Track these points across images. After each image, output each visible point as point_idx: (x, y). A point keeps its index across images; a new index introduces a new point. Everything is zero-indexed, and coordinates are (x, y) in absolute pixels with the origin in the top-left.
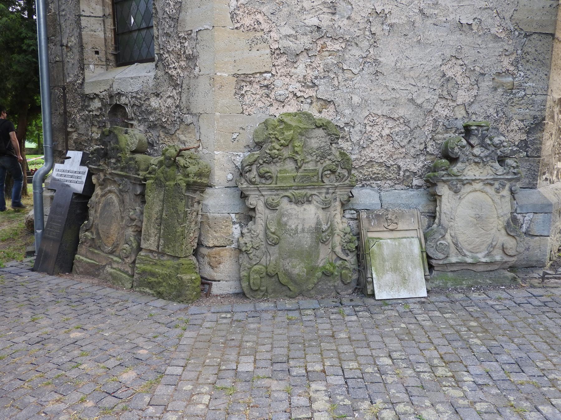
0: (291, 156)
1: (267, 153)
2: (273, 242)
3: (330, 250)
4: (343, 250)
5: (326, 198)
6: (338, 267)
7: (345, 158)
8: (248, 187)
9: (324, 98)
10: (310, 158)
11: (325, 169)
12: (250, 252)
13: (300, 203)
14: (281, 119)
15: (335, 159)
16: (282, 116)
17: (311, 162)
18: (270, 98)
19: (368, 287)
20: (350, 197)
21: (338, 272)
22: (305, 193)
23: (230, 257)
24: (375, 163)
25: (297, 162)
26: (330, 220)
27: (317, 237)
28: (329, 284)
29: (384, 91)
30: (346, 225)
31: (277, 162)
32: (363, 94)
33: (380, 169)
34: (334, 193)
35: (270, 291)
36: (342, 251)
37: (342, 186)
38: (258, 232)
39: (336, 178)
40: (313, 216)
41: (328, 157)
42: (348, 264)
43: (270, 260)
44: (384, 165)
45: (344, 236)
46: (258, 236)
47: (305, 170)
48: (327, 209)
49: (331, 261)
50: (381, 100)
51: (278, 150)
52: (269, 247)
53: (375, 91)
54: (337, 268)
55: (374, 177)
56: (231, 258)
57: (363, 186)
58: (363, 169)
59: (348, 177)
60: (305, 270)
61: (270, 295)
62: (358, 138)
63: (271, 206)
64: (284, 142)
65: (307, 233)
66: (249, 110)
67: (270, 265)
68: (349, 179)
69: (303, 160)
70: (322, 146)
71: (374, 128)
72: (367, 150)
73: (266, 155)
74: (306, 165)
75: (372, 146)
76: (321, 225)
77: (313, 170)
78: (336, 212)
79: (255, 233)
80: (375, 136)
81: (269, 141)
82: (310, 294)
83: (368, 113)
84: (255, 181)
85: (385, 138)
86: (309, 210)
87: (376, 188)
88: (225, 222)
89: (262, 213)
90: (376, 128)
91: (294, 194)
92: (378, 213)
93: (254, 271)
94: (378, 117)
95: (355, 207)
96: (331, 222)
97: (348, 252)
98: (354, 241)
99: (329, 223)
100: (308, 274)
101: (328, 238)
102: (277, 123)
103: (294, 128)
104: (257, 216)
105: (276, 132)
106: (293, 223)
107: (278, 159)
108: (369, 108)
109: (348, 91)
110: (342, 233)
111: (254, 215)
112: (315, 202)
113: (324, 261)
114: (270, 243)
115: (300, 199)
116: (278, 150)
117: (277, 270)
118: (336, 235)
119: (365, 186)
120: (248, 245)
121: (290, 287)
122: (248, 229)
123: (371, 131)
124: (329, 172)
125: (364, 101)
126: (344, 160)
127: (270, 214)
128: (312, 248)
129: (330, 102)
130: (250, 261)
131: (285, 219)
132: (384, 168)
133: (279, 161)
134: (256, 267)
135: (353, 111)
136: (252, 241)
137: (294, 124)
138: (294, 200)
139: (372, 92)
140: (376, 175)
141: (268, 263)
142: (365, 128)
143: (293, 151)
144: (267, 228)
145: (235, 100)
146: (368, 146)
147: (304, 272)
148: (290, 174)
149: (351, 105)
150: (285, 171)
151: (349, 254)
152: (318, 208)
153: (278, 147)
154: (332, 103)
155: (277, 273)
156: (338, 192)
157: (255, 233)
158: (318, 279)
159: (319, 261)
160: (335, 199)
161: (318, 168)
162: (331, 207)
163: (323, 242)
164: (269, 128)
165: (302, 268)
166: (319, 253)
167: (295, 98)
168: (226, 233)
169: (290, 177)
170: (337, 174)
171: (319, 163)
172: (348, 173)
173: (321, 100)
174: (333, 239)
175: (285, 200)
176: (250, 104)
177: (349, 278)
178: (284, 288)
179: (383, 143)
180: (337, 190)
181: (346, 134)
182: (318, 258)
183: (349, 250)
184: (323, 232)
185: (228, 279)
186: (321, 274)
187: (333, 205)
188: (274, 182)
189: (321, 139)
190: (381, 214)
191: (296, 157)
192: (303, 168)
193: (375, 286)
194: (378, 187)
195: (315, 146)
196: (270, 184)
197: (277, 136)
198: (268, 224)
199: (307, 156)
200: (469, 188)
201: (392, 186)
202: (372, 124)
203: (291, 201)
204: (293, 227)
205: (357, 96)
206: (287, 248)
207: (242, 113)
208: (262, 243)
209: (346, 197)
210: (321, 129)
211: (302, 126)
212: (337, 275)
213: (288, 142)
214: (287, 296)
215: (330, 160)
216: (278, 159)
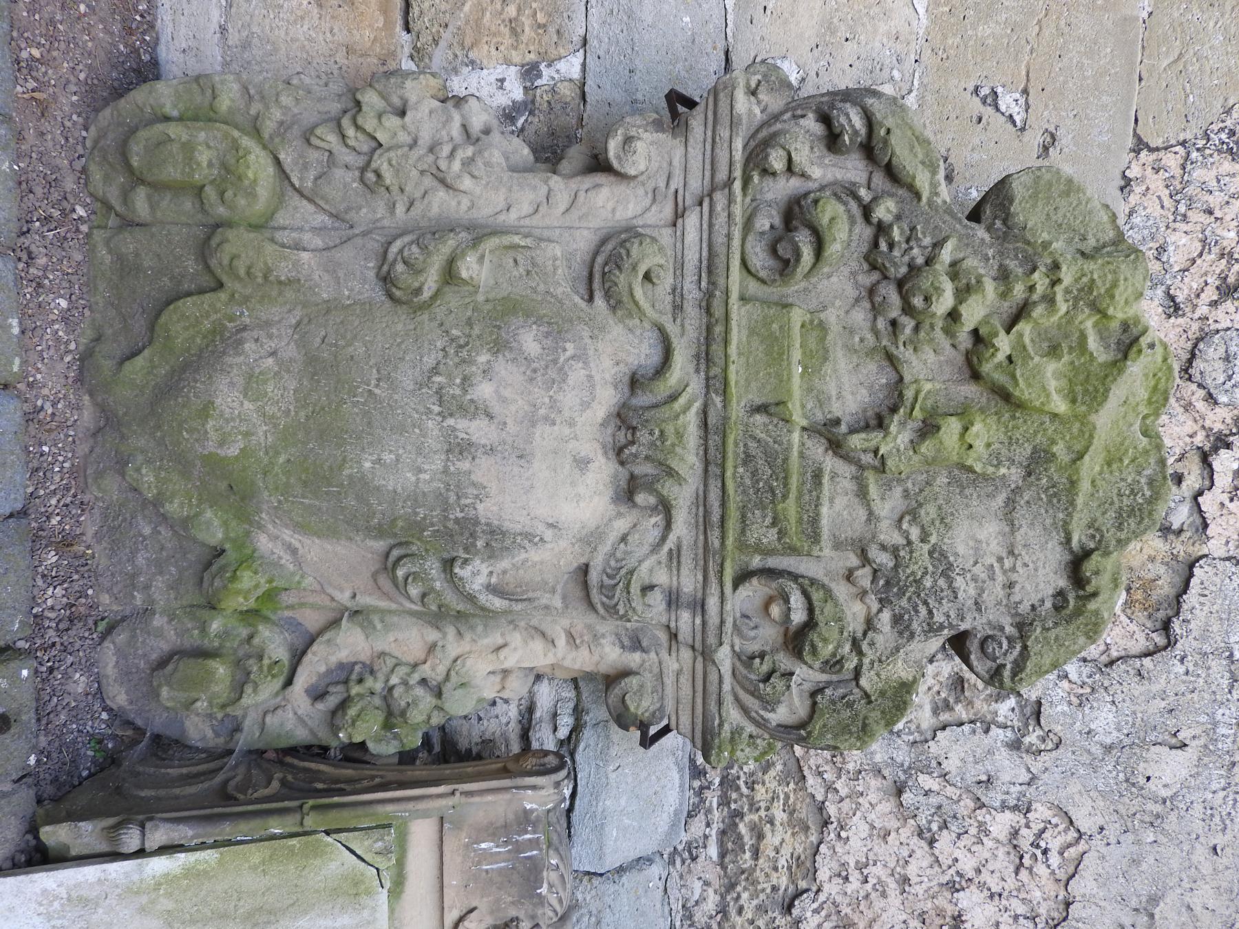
0: (909, 394)
1: (938, 245)
2: (400, 267)
3: (344, 597)
4: (345, 674)
5: (647, 589)
6: (251, 637)
7: (876, 715)
8: (734, 123)
9: (1191, 598)
10: (887, 506)
11: (817, 596)
12: (350, 132)
13: (622, 437)
14: (1144, 341)
15: (870, 655)
16: (1159, 350)
17: (862, 514)
18: (1214, 304)
19: (86, 826)
20: (643, 726)
21: (225, 634)
22: (682, 469)
23: (349, 50)
24: (814, 838)
25: (867, 427)
26: (518, 607)
27: (417, 527)
28: (159, 583)
29: (1206, 917)
30: (489, 694)
31: (876, 310)
32: (1198, 807)
33: (782, 862)
34: (673, 636)
35: (129, 243)
36: (341, 666)
37: (713, 688)
38: (467, 183)
39: (762, 656)
40: (543, 511)
41: (886, 616)
42: (268, 690)
43: (298, 247)
44: (803, 884)
45: (423, 682)
46: (443, 182)
47: (817, 476)
48: (578, 593)
49: (288, 599)
50: (1154, 900)
51: (953, 315)
52: (374, 244)
53: (1206, 869)
54: (244, 632)
55: (742, 828)
56: (340, 57)
57: (697, 773)
58: (783, 780)
59: (761, 724)
60: (233, 451)
61: (107, 242)
62: (951, 765)
63: (616, 261)
64: (1001, 357)
65: (446, 471)
66: (1156, 183)
67: (269, 248)
68: (750, 728)
69: (882, 468)
70: (959, 582)
71: (1001, 853)
72: (887, 806)
73: (927, 241)
74: (848, 485)
75: (905, 833)
76: (491, 554)
77: (815, 521)
78: (561, 641)
79: (456, 166)
80: (958, 854)
81: (1012, 264)
82: (100, 475)
83: (1085, 823)
84: (767, 172)
85: (941, 902)
86: (581, 489)
87: (685, 837)
88: (541, 18)
89: (575, 214)
90: (1003, 862)
91: (682, 400)
92: (550, 876)
93: (236, 146)
94: (1062, 875)
95: (588, 735)
96: (505, 612)
97: (332, 701)
98: (396, 736)
99: (498, 603)
100: (214, 463)
101: (414, 591)
102: (1118, 313)
103: (1082, 419)
104: (556, 181)
105: (1063, 307)
106: (507, 393)
107: (895, 313)
108: (1112, 832)
109: (1222, 730)
110: (442, 669)
111: (565, 166)
112: (622, 525)
113: (286, 560)
114: (394, 249)
115: (643, 436)
116: (953, 315)
117: (238, 286)
118: (432, 635)
119: (697, 784)
120: (392, 121)
121: (139, 361)
122: (487, 131)
123: (987, 833)
124: (798, 617)
125: (1158, 808)
126: (860, 706)
127: (568, 258)
128: (359, 498)
129: (1166, 626)
130: (296, 131)
131: (530, 341)
132: (783, 881)
133: (881, 324)
134: (258, 166)
135: (1108, 749)
136: (414, 144)
137: (1105, 419)
138: (643, 399)
139: (1201, 854)
140: (748, 841)
141: (283, 237)
142: (1004, 807)
143: (935, 408)
144: (479, 233)
145: (1218, 107)
146: (905, 814)
147: (222, 444)
148: (796, 381)
149: (1144, 744)
150: (817, 358)
151: (320, 706)
152: (591, 539)
153: (973, 313)
154: (1159, 639)
155: (220, 285)
156: (678, 662)
157: (456, 166)
158: (186, 522)
159: (287, 535)
160: (636, 644)
161: (827, 552)
162: (591, 618)
163: (388, 565)
164: (1090, 266)
165: (247, 434)
166: (329, 532)
167: (1200, 439)
168: (478, 22)
169: (783, 381)
170: (785, 661)
171: (854, 561)
172: (785, 728)
173: (1178, 580)
174: (410, 620)
175: (643, 353)
176: (1190, 190)
177: (182, 696)
178: (139, 325)
179: (919, 890)
180: (686, 654)
181: (978, 704)
182: (301, 528)
183: (343, 705)
184: (448, 564)
185: (234, 38)
186: (213, 542)
187: (607, 627)
188: (753, 287)
189: (1000, 578)
190: (544, 890)
191: (903, 424)
192: (830, 463)
193: (90, 873)
194: (689, 844)
195: (960, 543)
196: (744, 263)
197: (1038, 312)
198: (507, 240)
199: (898, 491)
200: (601, 196)
201: (690, 917)
202: (1025, 842)
203: (634, 382)
204: (484, 390)
205: (1184, 773)
206: (359, 349)
207: (1140, 145)
208: (400, 209)
209: (641, 706)
210: (1062, 583)
211: (1091, 466)
212: (203, 629)
213: (1000, 378)
214: (98, 339)
215: (870, 625)
216: (895, 313)
